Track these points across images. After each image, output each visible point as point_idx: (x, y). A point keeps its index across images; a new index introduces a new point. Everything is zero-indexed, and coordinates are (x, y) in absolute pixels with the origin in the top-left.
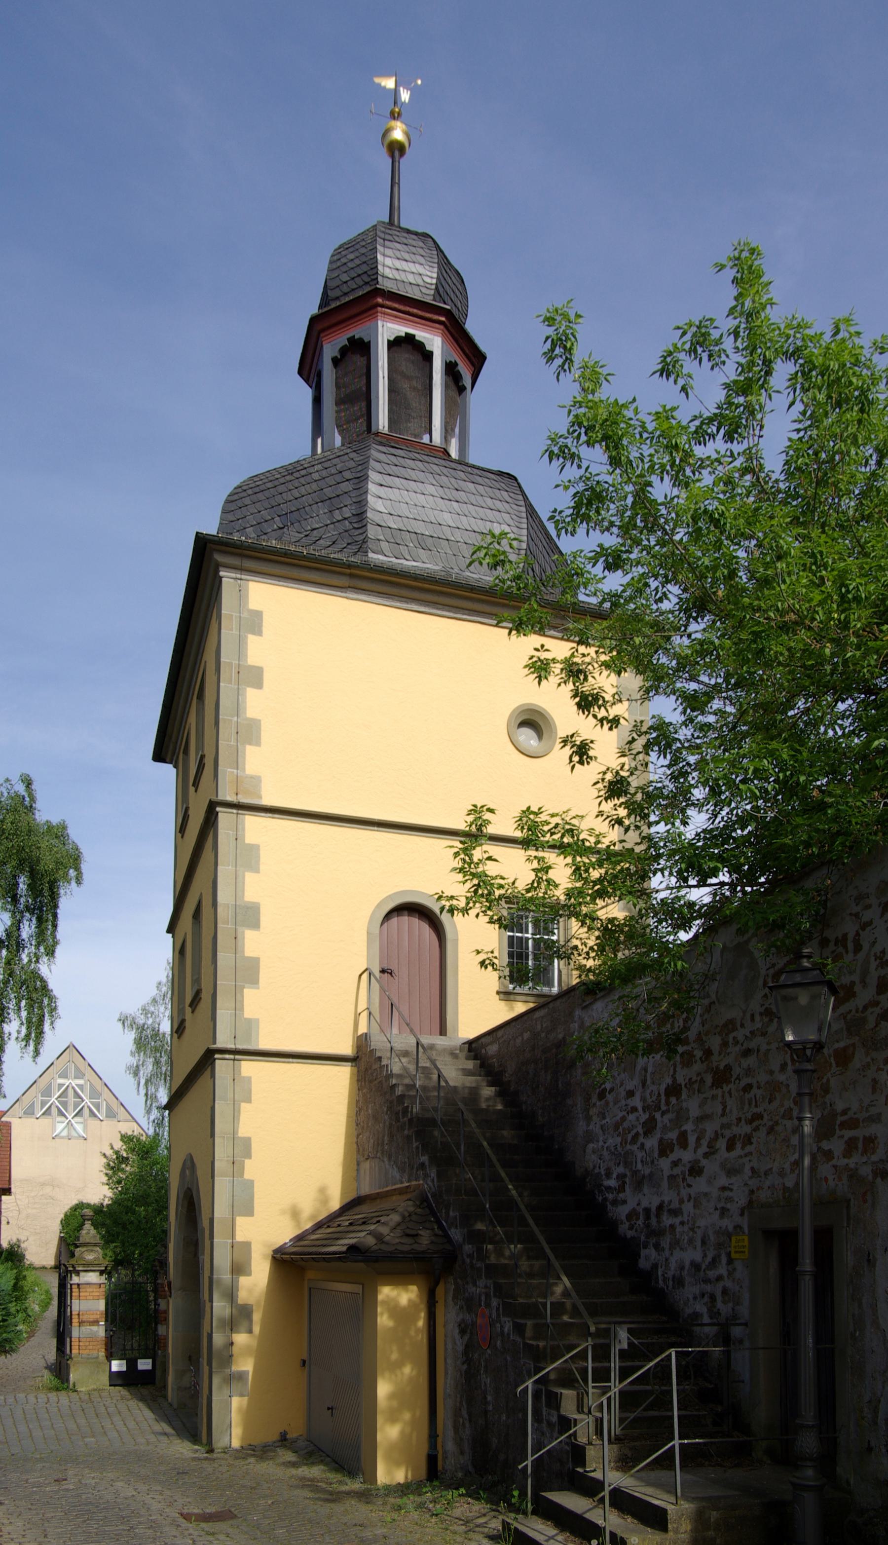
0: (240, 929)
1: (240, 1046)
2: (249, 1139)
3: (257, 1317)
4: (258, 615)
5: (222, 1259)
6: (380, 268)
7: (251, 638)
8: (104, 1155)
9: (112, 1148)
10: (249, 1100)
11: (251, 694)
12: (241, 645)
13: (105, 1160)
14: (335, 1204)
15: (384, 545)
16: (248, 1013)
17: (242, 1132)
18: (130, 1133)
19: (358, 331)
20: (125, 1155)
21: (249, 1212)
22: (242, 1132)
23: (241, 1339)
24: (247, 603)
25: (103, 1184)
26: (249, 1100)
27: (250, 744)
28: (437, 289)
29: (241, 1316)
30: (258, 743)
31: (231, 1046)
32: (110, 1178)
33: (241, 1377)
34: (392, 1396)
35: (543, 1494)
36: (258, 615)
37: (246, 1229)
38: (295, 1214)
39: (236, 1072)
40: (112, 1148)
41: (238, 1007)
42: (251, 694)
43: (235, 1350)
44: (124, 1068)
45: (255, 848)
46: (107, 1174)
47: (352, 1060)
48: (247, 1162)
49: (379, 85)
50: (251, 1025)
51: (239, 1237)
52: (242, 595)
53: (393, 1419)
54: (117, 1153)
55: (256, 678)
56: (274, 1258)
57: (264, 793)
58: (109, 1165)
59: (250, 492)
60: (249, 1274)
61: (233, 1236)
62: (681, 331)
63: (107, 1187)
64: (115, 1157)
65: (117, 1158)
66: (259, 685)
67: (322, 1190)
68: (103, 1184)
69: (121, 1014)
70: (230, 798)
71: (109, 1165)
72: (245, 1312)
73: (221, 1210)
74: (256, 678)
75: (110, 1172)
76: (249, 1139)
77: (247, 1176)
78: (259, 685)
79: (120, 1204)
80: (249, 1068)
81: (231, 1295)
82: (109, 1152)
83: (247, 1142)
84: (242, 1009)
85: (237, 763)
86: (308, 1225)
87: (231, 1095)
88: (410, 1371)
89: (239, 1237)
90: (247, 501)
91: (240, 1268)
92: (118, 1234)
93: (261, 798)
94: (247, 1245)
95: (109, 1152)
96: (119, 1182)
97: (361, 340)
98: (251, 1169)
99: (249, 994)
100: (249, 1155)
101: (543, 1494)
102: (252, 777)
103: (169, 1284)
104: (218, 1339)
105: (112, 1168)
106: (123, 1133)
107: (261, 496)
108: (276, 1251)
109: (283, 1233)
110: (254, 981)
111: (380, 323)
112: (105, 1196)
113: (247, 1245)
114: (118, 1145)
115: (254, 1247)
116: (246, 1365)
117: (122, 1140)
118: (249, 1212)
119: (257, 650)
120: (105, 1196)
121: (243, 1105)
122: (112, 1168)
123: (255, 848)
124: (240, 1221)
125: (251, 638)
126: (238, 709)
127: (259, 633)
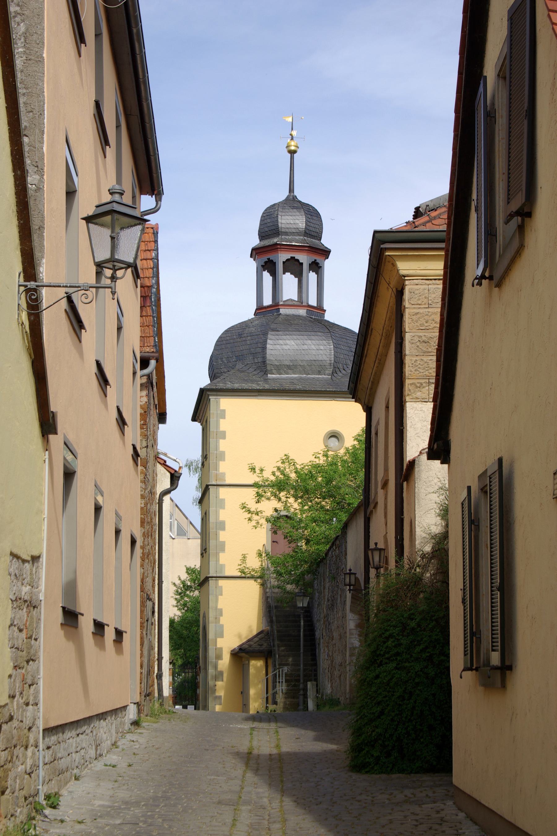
0: (218, 531)
1: (218, 575)
2: (222, 609)
3: (225, 675)
4: (224, 411)
5: (211, 653)
6: (280, 225)
7: (221, 420)
8: (174, 584)
9: (180, 579)
10: (222, 595)
11: (221, 441)
12: (217, 514)
13: (175, 588)
14: (255, 632)
15: (274, 371)
16: (221, 562)
17: (219, 607)
18: (193, 567)
19: (272, 257)
20: (189, 584)
21: (222, 636)
22: (219, 607)
23: (219, 684)
24: (220, 407)
25: (174, 606)
26: (222, 595)
27: (221, 461)
28: (305, 232)
29: (219, 676)
30: (224, 460)
31: (215, 575)
32: (178, 601)
33: (220, 697)
34: (255, 694)
35: (334, 747)
36: (224, 411)
37: (221, 643)
38: (240, 636)
39: (217, 584)
40: (180, 579)
41: (217, 560)
42: (221, 441)
43: (217, 687)
44: (191, 501)
45: (223, 500)
46: (176, 599)
47: (260, 577)
48: (221, 618)
49: (285, 120)
50: (223, 566)
51: (218, 646)
52: (218, 404)
53: (255, 701)
54: (183, 583)
55: (223, 435)
56: (231, 654)
57: (226, 479)
58: (177, 591)
59: (224, 342)
60: (222, 659)
61: (216, 645)
62: (551, 14)
63: (176, 608)
64: (182, 586)
65: (184, 586)
66: (224, 438)
67: (250, 627)
68: (174, 606)
69: (187, 460)
70: (214, 483)
71: (177, 591)
72: (221, 673)
73: (211, 635)
74: (223, 435)
75: (178, 597)
76: (222, 609)
77: (221, 623)
78: (224, 438)
79: (182, 626)
80: (221, 582)
81: (216, 667)
82: (178, 582)
83: (221, 610)
84: (219, 561)
85: (216, 469)
86: (244, 641)
87: (215, 593)
88: (261, 686)
89: (218, 646)
90: (223, 347)
91: (219, 657)
92: (181, 644)
93: (225, 480)
94: (221, 649)
95: (178, 582)
96: (185, 605)
97: (272, 261)
98: (223, 620)
99: (221, 555)
100: (222, 615)
101: (334, 747)
102: (222, 473)
103: (200, 667)
104: (211, 683)
105: (180, 594)
106: (188, 566)
107: (228, 346)
108: (232, 651)
109: (235, 644)
110: (223, 550)
111: (280, 255)
112: (175, 615)
113: (221, 649)
114: (184, 576)
115: (224, 649)
116: (221, 693)
117: (187, 572)
118: (222, 636)
119: (223, 425)
120: (175, 615)
121: (220, 597)
122: (180, 594)
123: (223, 500)
124: (218, 640)
125: (221, 420)
126: (217, 447)
127: (224, 418)
